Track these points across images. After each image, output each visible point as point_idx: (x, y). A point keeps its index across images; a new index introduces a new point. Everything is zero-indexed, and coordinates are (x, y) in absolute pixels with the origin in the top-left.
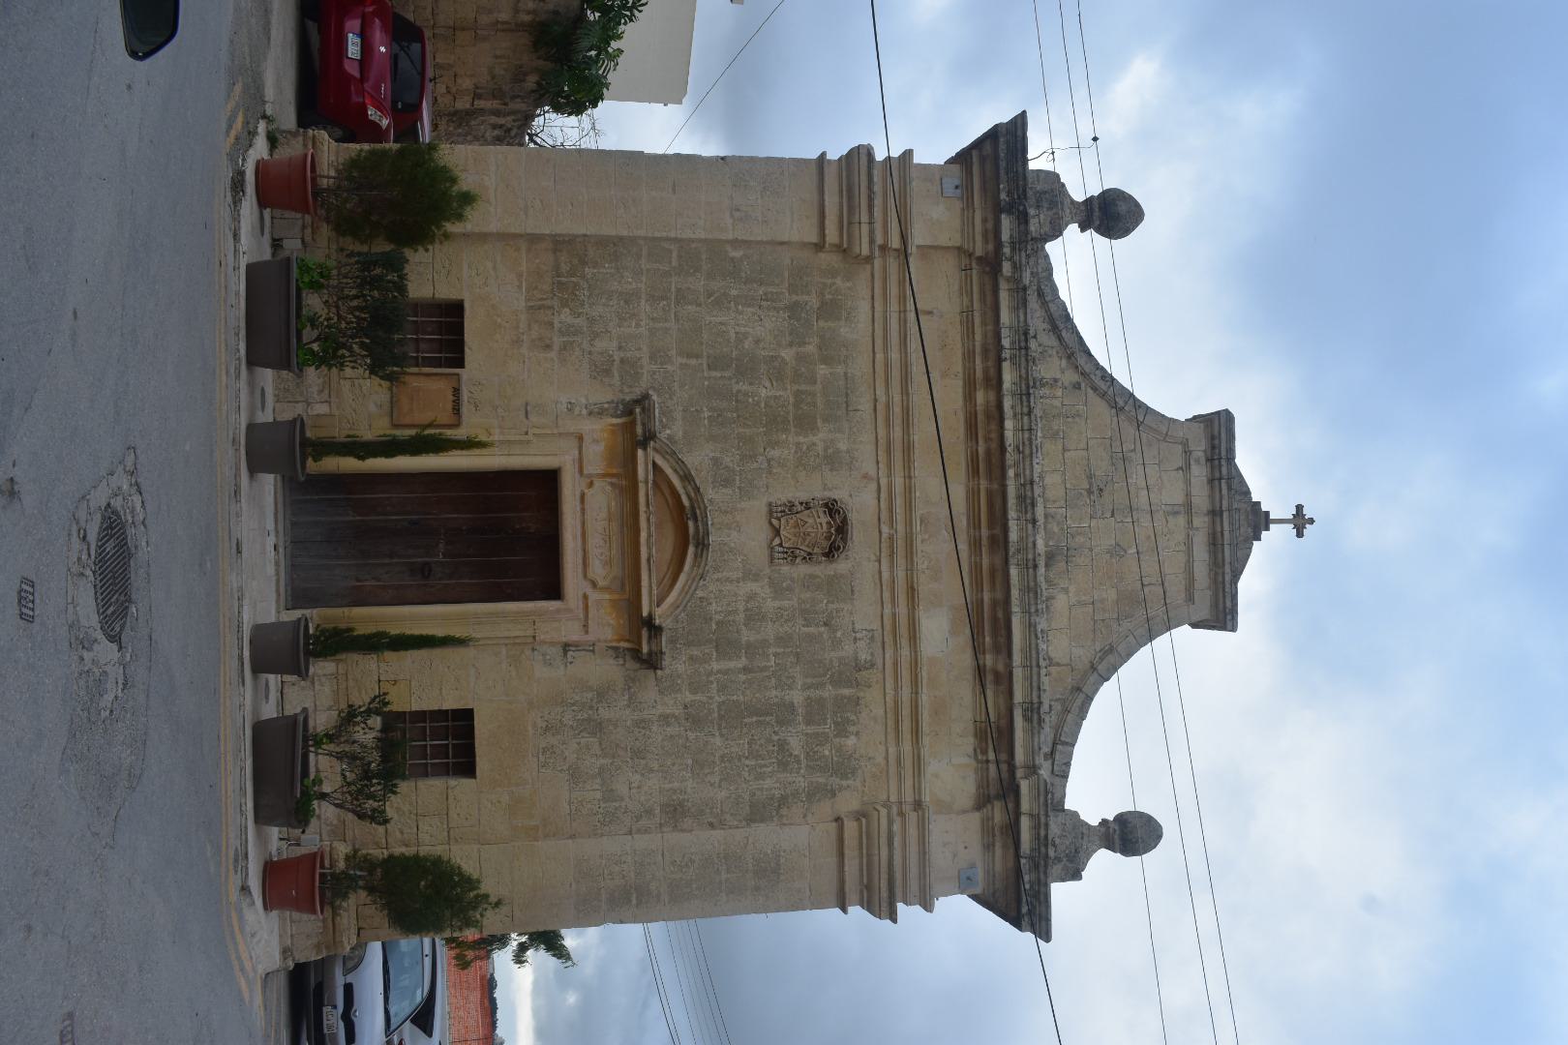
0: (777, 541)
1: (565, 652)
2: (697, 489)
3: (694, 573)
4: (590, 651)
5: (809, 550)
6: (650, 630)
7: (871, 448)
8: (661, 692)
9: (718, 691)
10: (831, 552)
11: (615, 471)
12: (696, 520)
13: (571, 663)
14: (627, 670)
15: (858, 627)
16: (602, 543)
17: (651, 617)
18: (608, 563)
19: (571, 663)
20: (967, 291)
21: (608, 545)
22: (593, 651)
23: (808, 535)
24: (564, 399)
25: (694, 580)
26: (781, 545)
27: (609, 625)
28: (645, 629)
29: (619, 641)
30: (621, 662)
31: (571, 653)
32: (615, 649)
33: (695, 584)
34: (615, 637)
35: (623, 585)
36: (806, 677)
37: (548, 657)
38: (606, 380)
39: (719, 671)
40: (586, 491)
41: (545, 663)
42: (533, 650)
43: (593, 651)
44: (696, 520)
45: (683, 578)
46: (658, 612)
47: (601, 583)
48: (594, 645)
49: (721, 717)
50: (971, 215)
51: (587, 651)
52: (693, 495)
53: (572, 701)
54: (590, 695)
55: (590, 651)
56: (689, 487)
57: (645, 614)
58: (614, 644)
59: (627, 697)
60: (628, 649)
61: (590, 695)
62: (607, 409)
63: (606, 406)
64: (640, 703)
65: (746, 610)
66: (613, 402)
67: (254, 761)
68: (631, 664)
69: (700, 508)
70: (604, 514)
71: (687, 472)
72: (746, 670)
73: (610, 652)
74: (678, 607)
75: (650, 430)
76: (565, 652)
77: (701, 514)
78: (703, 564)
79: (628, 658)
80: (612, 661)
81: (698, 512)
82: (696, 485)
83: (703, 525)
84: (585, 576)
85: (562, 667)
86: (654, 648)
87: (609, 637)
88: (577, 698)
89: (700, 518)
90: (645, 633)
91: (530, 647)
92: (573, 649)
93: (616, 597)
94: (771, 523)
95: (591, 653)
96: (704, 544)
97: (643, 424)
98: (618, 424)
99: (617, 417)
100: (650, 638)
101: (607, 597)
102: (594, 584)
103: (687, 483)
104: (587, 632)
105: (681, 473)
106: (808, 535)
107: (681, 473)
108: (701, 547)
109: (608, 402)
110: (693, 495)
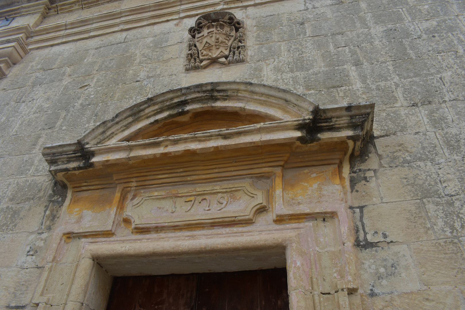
0: (223, 60)
1: (369, 245)
2: (150, 101)
3: (246, 94)
4: (362, 212)
5: (232, 39)
6: (321, 130)
7: (156, 27)
8: (403, 129)
9: (386, 80)
10: (236, 25)
11: (118, 195)
12: (185, 103)
13: (385, 236)
14: (381, 165)
15: (303, 7)
16: (205, 204)
17: (299, 127)
18: (232, 193)
19: (385, 236)
20: (71, 7)
21: (207, 197)
22: (361, 208)
23: (218, 39)
24: (23, 259)
25: (253, 92)
26: (226, 57)
27: (320, 189)
28: (319, 135)
29: (341, 178)
30: (371, 173)
31: (369, 238)
32: (353, 182)
33: (257, 89)
34: (338, 181)
35: (261, 177)
36: (355, 27)
37: (382, 270)
38: (22, 214)
39: (364, 81)
40: (133, 226)
41: (393, 274)
42: (372, 294)
43: (361, 208)
44: (185, 103)
45: (252, 107)
46: (288, 118)
47: (260, 199)
48: (351, 208)
49: (417, 75)
50: (25, 10)
51: (361, 217)
52: (156, 107)
53: (448, 230)
54: (431, 207)
55: (362, 212)
56: (147, 111)
57: (298, 134)
58: (347, 183)
59: (422, 164)
60: (352, 167)
61: (431, 207)
62: (52, 211)
63: (48, 212)
64: (424, 148)
65: (292, 71)
66: (47, 207)
67: (208, 273)
68: (372, 162)
69: (172, 99)
70: (167, 204)
71: (128, 113)
72: (357, 64)
73: (357, 187)
74: (286, 101)
75: (75, 152)
76: (369, 245)
77: (178, 97)
78: (234, 87)
79: (363, 167)
80: (373, 184)
81: (176, 100)
82: (145, 102)
83: (190, 93)
84: (248, 222)
85: (395, 248)
86: (344, 121)
87: (339, 187)
88: (440, 223)
89: (183, 98)
90: (325, 136)
91: (369, 300)
92: (361, 232)
93: (278, 181)
94: (206, 67)
95: (365, 210)
96: (212, 90)
97: (69, 161)
98: (72, 196)
99: (63, 201)
100: (331, 129)
101: (278, 192)
102: (262, 210)
103: (142, 114)
104: (333, 215)
105: (130, 119)
106: (218, 39)
107: (130, 119)
108: (216, 94)
109: (45, 212)
110: (156, 107)
